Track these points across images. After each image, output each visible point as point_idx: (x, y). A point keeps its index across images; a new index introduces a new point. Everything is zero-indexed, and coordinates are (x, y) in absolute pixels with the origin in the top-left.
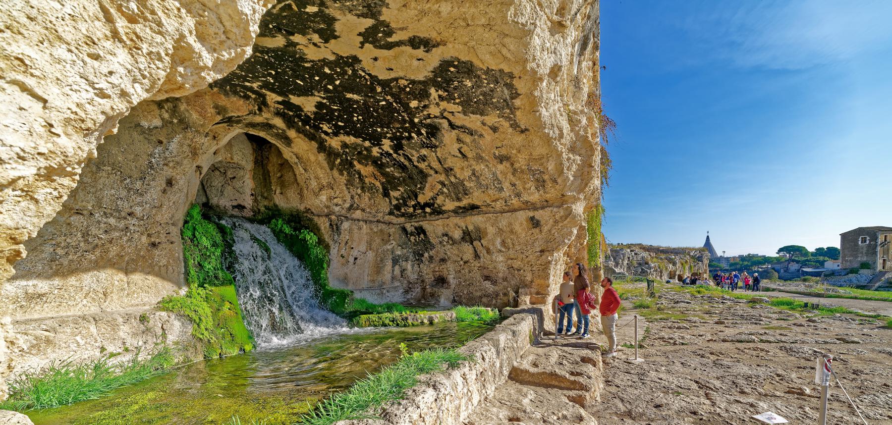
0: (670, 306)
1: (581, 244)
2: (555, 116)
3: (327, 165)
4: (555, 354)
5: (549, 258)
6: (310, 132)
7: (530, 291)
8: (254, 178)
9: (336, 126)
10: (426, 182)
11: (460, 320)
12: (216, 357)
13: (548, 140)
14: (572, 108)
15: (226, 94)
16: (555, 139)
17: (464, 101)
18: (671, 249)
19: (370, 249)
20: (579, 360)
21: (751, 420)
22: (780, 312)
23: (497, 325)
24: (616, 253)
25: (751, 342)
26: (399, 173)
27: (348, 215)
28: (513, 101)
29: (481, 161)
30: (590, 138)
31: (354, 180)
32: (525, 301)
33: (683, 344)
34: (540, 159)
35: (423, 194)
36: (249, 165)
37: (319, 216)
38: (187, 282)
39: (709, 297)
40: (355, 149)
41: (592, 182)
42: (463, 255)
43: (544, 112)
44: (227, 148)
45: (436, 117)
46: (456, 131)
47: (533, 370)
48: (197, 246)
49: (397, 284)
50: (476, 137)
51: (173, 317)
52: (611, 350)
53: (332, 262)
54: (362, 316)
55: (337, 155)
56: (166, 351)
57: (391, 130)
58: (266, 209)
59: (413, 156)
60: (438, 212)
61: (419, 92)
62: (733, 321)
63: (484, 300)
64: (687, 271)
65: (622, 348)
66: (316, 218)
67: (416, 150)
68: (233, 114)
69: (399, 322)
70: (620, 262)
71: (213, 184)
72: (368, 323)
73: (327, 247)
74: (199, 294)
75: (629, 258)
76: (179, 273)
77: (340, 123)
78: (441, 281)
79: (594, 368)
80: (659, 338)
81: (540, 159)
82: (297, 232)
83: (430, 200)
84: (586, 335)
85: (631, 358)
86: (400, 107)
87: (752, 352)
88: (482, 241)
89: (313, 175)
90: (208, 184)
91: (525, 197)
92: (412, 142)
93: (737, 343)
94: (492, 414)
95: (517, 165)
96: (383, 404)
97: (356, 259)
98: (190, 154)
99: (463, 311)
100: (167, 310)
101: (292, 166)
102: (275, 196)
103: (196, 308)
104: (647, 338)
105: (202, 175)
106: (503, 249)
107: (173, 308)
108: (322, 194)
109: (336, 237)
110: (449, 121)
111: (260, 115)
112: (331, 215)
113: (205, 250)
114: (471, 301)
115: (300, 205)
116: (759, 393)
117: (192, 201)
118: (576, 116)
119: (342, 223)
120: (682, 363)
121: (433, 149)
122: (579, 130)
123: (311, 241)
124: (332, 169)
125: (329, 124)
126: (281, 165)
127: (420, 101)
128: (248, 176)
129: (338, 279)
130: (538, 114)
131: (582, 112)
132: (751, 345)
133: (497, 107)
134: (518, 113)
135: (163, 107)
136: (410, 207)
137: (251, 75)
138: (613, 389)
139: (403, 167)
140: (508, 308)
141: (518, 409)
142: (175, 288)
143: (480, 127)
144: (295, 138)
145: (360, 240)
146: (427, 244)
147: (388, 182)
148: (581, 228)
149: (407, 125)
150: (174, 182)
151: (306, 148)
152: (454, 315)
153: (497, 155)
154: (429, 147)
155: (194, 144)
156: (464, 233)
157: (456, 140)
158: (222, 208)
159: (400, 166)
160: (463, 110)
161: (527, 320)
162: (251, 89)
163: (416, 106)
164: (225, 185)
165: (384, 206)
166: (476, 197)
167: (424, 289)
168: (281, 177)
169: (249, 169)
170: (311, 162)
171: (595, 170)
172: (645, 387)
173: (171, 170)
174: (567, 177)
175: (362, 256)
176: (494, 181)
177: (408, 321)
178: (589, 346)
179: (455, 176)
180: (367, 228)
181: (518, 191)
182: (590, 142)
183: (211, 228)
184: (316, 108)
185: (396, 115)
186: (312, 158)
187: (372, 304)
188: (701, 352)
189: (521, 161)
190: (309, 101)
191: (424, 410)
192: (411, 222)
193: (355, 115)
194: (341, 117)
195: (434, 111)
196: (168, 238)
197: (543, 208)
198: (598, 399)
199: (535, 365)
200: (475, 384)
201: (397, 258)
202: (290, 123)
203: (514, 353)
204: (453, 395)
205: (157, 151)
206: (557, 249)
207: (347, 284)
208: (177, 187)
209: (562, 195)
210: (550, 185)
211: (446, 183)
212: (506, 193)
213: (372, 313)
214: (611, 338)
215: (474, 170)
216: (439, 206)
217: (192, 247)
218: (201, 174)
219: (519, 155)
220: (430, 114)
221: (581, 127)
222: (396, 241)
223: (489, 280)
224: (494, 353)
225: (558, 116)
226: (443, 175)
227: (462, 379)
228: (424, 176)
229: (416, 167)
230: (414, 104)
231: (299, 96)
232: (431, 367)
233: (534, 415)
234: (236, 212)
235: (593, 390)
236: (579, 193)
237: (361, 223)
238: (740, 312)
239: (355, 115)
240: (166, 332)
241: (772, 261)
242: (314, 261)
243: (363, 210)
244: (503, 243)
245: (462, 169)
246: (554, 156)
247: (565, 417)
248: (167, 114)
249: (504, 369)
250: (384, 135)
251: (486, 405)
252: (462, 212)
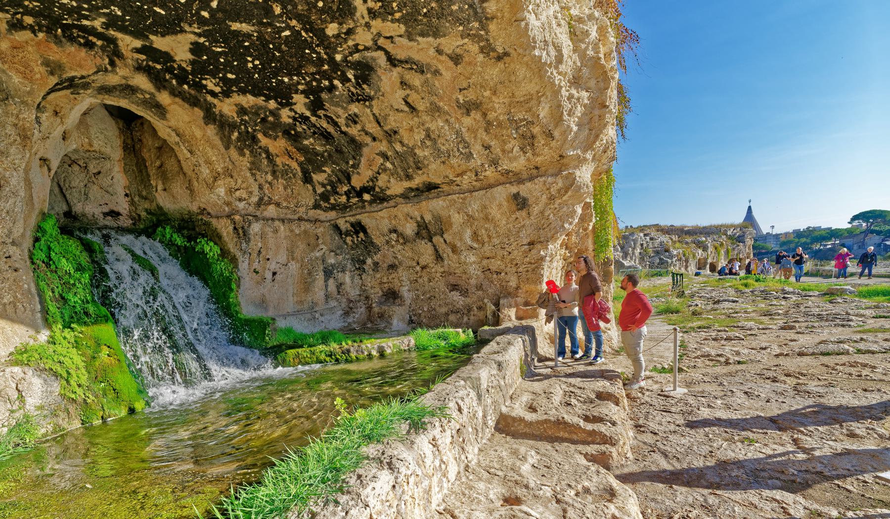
0: (709, 308)
1: (585, 229)
2: (550, 27)
3: (220, 142)
4: (558, 390)
5: (542, 253)
6: (190, 94)
7: (516, 301)
8: (126, 172)
9: (224, 80)
10: (361, 156)
11: (420, 348)
12: (97, 422)
13: (539, 68)
14: (574, 12)
15: (58, 41)
16: (550, 66)
17: (408, 14)
18: (700, 228)
19: (293, 259)
20: (593, 396)
21: (878, 480)
22: (877, 307)
23: (475, 356)
24: (626, 240)
25: (842, 354)
26: (322, 145)
27: (258, 213)
28: (484, 5)
29: (437, 114)
30: (603, 62)
31: (261, 162)
32: (509, 316)
33: (739, 363)
34: (527, 102)
35: (358, 173)
36: (117, 154)
37: (218, 217)
38: (48, 324)
39: (763, 291)
40: (257, 114)
41: (605, 131)
42: (419, 257)
43: (532, 19)
45: (367, 49)
46: (399, 69)
47: (530, 417)
48: (56, 272)
49: (333, 303)
50: (429, 76)
51: (30, 373)
52: (636, 377)
53: (242, 281)
55: (233, 126)
56: (27, 419)
57: (304, 79)
58: (148, 213)
59: (339, 117)
60: (381, 198)
61: (338, 7)
62: (806, 324)
63: (452, 318)
64: (723, 257)
65: (651, 373)
66: (214, 222)
67: (343, 108)
68: (73, 74)
69: (338, 356)
70: (630, 252)
71: (73, 184)
72: (297, 361)
73: (234, 260)
74: (65, 338)
75: (642, 245)
76: (33, 311)
77: (230, 76)
78: (392, 296)
79: (617, 408)
80: (702, 356)
81: (527, 102)
82: (192, 243)
83: (368, 182)
84: (599, 359)
85: (668, 388)
86: (311, 38)
87: (848, 370)
88: (445, 236)
90: (67, 186)
91: (505, 165)
92: (335, 95)
93: (821, 357)
94: (478, 494)
95: (491, 116)
96: (312, 504)
97: (274, 274)
98: (18, 138)
99: (424, 336)
100: (17, 363)
101: (173, 149)
102: (157, 195)
103: (62, 358)
104: (685, 357)
105: (53, 172)
106: (476, 245)
107: (29, 361)
108: (219, 186)
109: (244, 245)
110: (387, 53)
111: (114, 71)
112: (233, 214)
113: (67, 277)
114: (434, 321)
115: (192, 205)
116: (879, 435)
118: (581, 25)
119: (249, 226)
120: (746, 393)
121: (367, 103)
122: (587, 49)
123: (211, 254)
125: (214, 78)
126: (160, 149)
127: (340, 24)
128: (117, 169)
130: (523, 24)
131: (591, 17)
132: (844, 359)
133: (458, 19)
134: (492, 27)
136: (342, 195)
137: (86, 6)
138: (649, 438)
139: (326, 137)
140: (486, 328)
141: (516, 482)
142: (32, 332)
143: (433, 59)
144: (169, 105)
145: (278, 247)
146: (369, 246)
147: (309, 161)
148: (587, 206)
149: (326, 67)
151: (187, 118)
152: (413, 342)
153: (462, 102)
154: (361, 100)
155: (21, 123)
156: (419, 226)
157: (398, 84)
158: (90, 217)
159: (322, 134)
160: (406, 31)
161: (515, 344)
162: (92, 31)
163: (336, 32)
164: (89, 185)
165: (307, 197)
166: (434, 172)
167: (369, 308)
168: (161, 166)
169: (117, 159)
170: (197, 139)
171: (610, 112)
172: (697, 433)
174: (569, 126)
175: (282, 270)
176: (458, 144)
177: (351, 354)
178: (604, 375)
179: (401, 142)
180: (285, 229)
181: (494, 156)
182: (603, 66)
183: (73, 246)
184: (193, 54)
185: (307, 51)
186: (198, 133)
187: (301, 334)
188: (770, 374)
189: (498, 109)
190: (179, 42)
191: (376, 508)
192: (345, 217)
193: (249, 59)
194: (228, 65)
195: (363, 38)
197: (531, 179)
198: (629, 455)
199: (532, 409)
200: (450, 450)
201: (331, 268)
202: (159, 81)
203: (501, 394)
204: (420, 473)
206: (553, 238)
207: (266, 309)
208: (8, 189)
209: (560, 156)
210: (543, 142)
211: (389, 153)
212: (477, 160)
213: (301, 347)
214: (636, 362)
215: (428, 130)
216: (382, 190)
217: (48, 273)
218: (49, 170)
219: (494, 98)
220: (358, 45)
221: (589, 42)
222: (326, 245)
223: (457, 290)
224: (475, 398)
225: (555, 26)
226: (385, 143)
227: (431, 446)
228: (356, 146)
229: (345, 133)
230: (332, 29)
231: (163, 36)
232: (384, 432)
233: (541, 492)
234: (109, 222)
235: (621, 443)
236: (585, 151)
237: (277, 223)
238: (816, 311)
239: (249, 59)
240: (24, 394)
241: (841, 235)
242: (219, 282)
243: (278, 205)
244: (475, 236)
245: (411, 130)
246: (549, 94)
247: (587, 491)
249: (489, 418)
250: (294, 88)
251: (468, 478)
252: (415, 196)
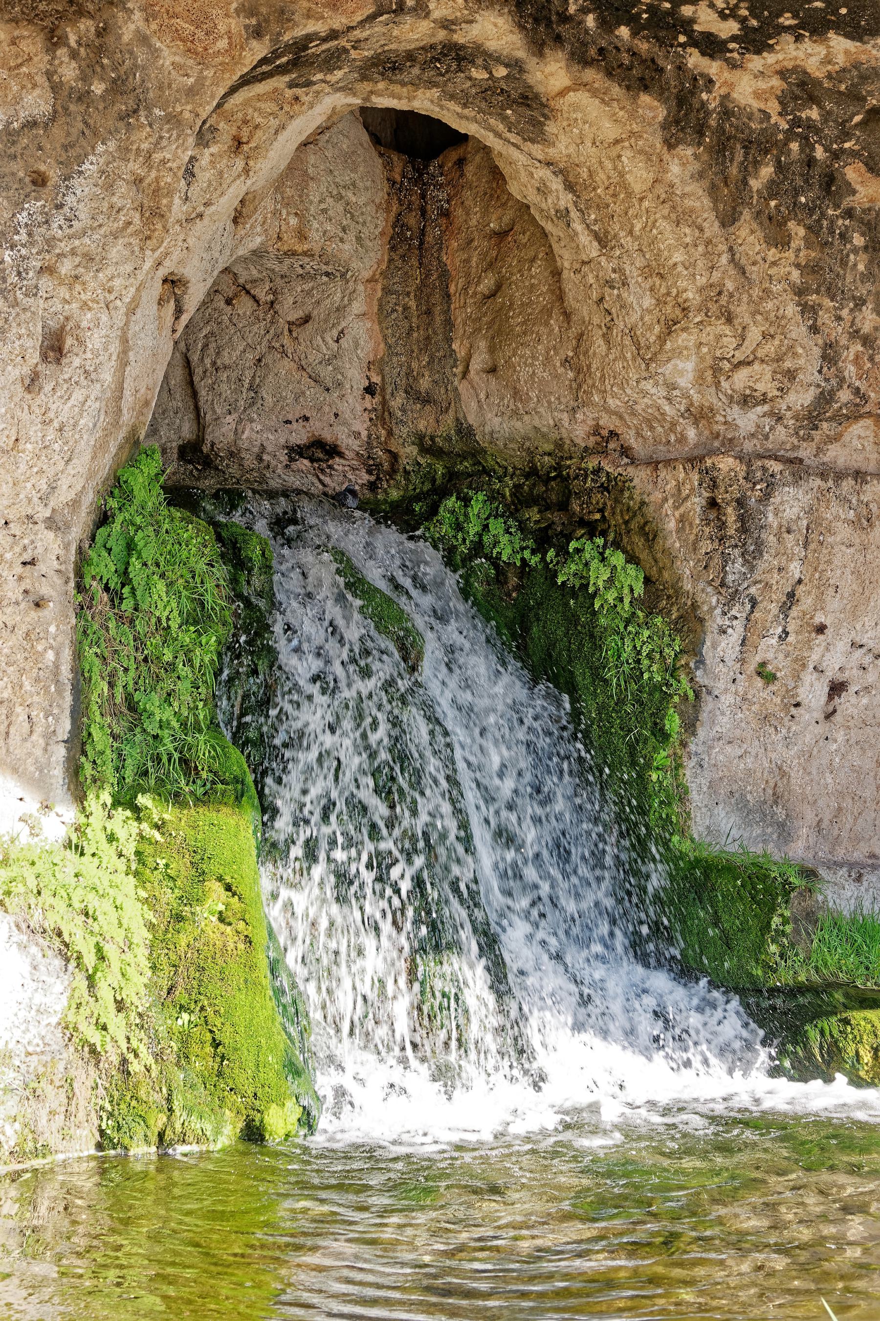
3: (707, 202)
8: (383, 313)
27: (806, 452)
31: (844, 263)
37: (654, 464)
44: (289, 192)
53: (708, 704)
54: (858, 1016)
58: (424, 450)
66: (639, 477)
68: (312, 27)
74: (111, 838)
89: (640, 262)
90: (208, 361)
97: (837, 688)
98: (136, 218)
101: (545, 234)
102: (463, 388)
103: (93, 902)
105: (185, 319)
108: (678, 353)
109: (737, 566)
112: (712, 453)
115: (573, 419)
117: (134, 430)
119: (767, 496)
123: (611, 596)
124: (728, 219)
129: (742, 806)
135: (62, 41)
144: (562, 93)
150: (69, 341)
151: (609, 130)
155: (153, 174)
164: (268, 359)
169: (366, 274)
170: (629, 195)
173: (64, 292)
196: (26, 584)
205: (23, 218)
208: (77, 362)
217: (112, 625)
218: (179, 311)
248: (74, 64)
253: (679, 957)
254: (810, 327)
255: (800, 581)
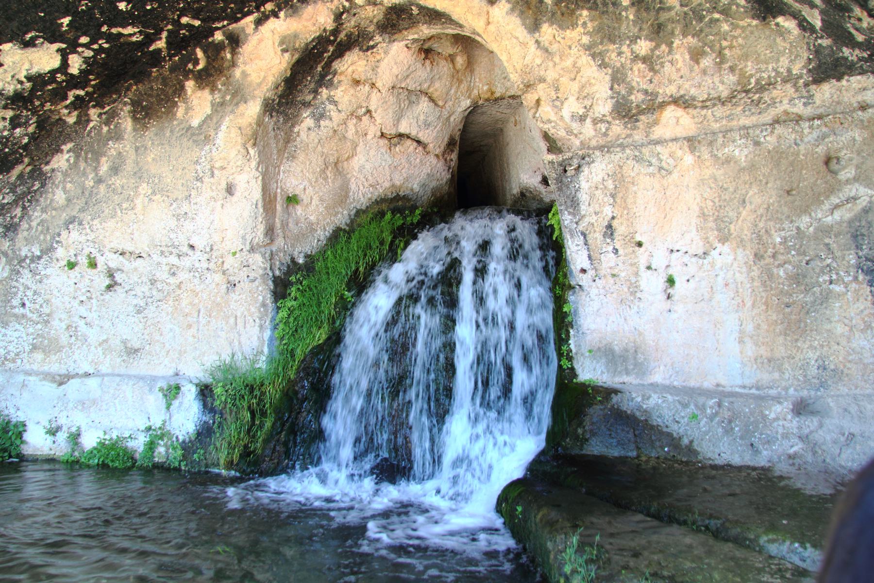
253: (238, 474)
254: (600, 66)
255: (613, 218)
